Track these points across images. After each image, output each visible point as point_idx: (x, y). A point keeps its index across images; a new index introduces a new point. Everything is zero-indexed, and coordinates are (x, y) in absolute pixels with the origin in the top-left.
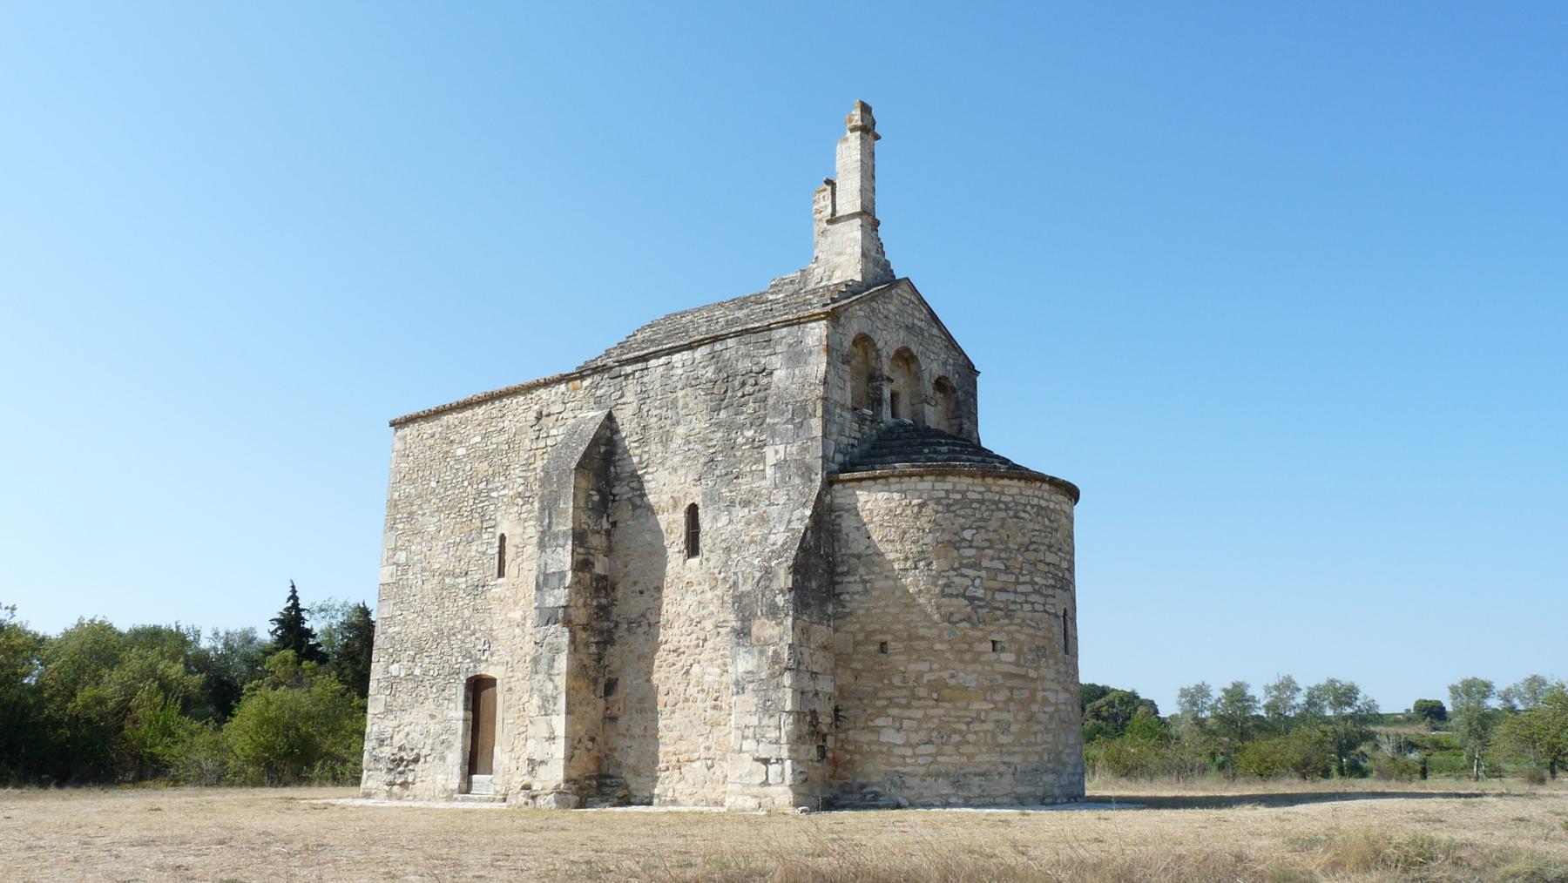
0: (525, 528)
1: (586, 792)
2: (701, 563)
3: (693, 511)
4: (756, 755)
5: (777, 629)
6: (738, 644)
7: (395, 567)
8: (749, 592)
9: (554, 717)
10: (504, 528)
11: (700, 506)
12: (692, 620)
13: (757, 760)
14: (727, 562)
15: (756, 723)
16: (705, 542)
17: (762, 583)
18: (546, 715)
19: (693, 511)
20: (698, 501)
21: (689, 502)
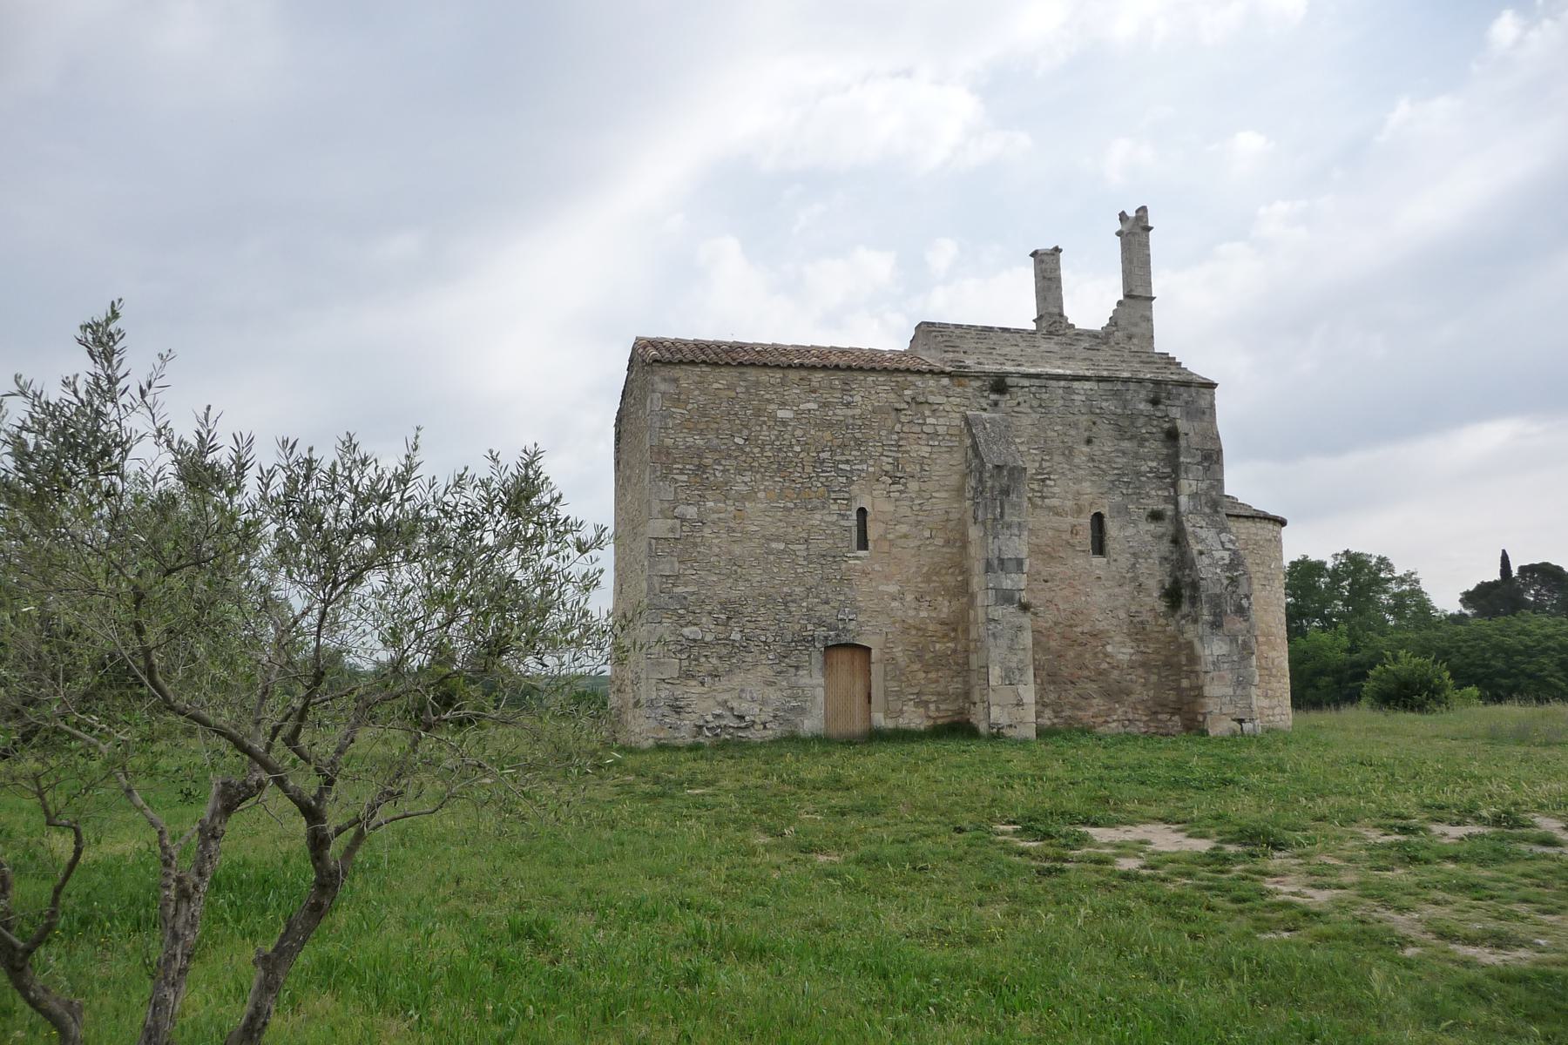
0: (896, 507)
1: (47, 542)
2: (1108, 563)
3: (1098, 519)
4: (1234, 717)
5: (1244, 624)
6: (1212, 634)
7: (678, 522)
8: (288, 477)
9: (1021, 688)
10: (865, 502)
11: (1107, 515)
12: (92, 464)
13: (1234, 720)
14: (1134, 564)
15: (1232, 693)
16: (1111, 545)
17: (1230, 588)
18: (1010, 684)
19: (1098, 519)
20: (1105, 511)
21: (1094, 511)
